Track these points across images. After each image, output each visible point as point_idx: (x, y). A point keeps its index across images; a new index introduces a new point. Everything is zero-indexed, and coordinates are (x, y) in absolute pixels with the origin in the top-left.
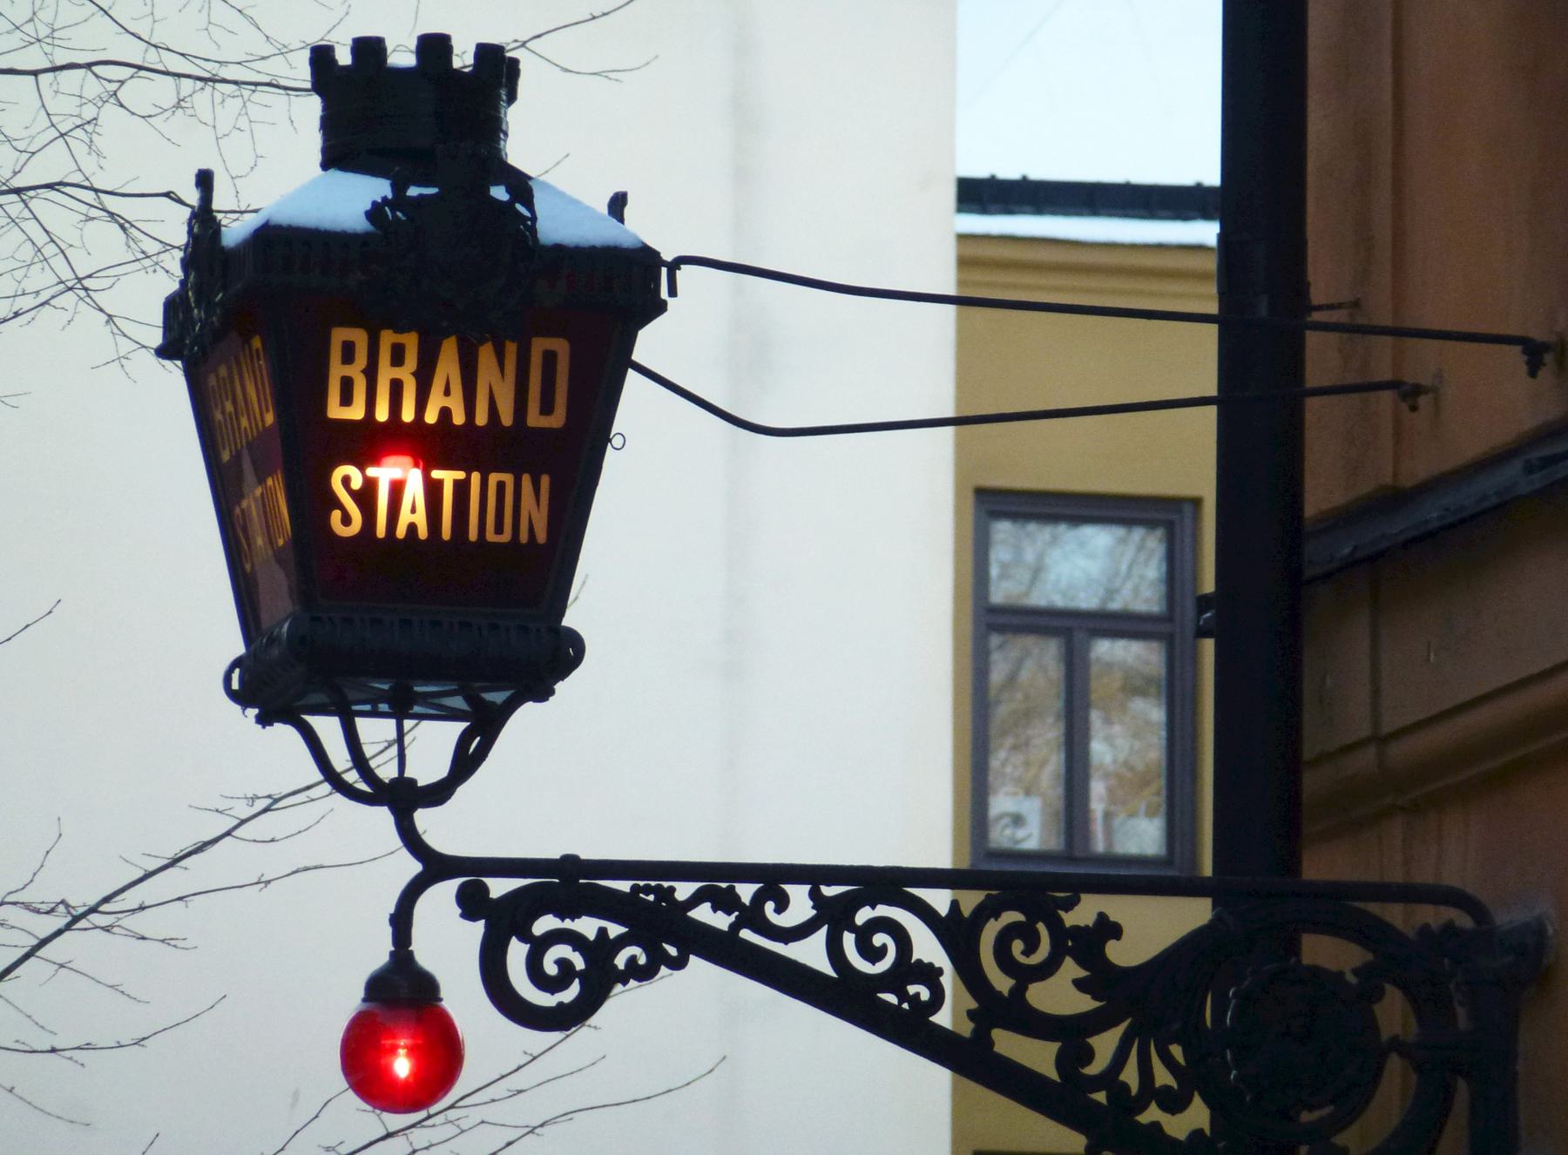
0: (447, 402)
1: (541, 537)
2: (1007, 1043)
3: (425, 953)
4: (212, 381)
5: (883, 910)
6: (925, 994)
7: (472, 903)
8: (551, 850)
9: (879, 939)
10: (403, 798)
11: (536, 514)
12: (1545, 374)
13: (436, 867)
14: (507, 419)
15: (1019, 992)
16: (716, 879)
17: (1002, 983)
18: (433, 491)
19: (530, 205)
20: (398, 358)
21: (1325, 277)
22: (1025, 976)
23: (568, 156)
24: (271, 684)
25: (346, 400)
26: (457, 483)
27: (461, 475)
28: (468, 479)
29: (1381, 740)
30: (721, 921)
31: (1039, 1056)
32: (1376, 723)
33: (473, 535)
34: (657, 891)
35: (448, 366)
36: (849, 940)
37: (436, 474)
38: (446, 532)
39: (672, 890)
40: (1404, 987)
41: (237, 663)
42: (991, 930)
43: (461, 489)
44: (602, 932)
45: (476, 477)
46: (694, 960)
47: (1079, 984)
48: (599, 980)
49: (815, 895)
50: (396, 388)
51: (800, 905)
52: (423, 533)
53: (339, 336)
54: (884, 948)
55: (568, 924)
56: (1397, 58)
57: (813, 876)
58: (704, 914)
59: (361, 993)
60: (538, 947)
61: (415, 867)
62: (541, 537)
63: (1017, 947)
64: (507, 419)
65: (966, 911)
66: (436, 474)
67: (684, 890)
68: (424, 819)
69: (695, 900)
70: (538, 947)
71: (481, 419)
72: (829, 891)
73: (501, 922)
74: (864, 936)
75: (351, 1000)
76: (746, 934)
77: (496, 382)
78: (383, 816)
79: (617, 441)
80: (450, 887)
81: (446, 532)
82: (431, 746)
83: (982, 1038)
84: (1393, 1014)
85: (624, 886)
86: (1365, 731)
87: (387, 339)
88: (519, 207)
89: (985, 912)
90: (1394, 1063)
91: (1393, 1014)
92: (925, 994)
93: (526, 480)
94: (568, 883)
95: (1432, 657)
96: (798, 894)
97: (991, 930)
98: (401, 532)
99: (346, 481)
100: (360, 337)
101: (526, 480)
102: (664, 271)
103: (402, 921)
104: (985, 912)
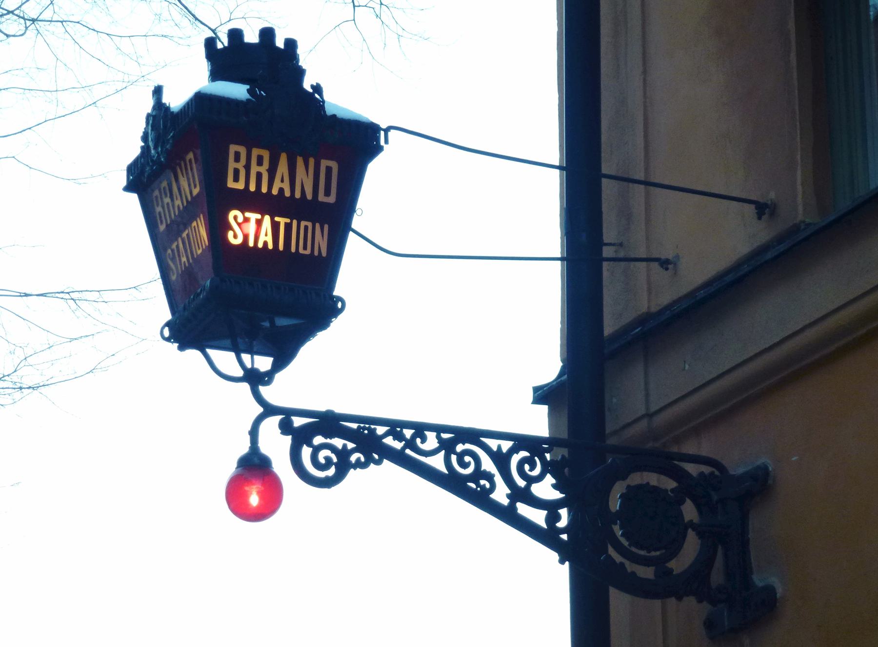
0: (282, 185)
1: (324, 254)
2: (523, 509)
3: (264, 448)
4: (159, 209)
5: (468, 446)
6: (488, 485)
7: (286, 427)
8: (322, 408)
9: (467, 459)
10: (255, 379)
11: (322, 243)
12: (765, 217)
13: (269, 410)
14: (309, 196)
15: (528, 487)
16: (395, 427)
17: (521, 483)
18: (275, 226)
19: (321, 94)
20: (260, 162)
21: (609, 234)
22: (530, 480)
23: (340, 81)
24: (191, 328)
25: (236, 179)
26: (286, 224)
27: (288, 220)
28: (292, 222)
29: (649, 416)
30: (398, 445)
31: (538, 517)
32: (647, 408)
33: (293, 250)
34: (369, 429)
35: (283, 168)
36: (454, 458)
37: (277, 219)
38: (281, 247)
39: (375, 429)
40: (694, 501)
41: (168, 324)
42: (515, 459)
43: (288, 227)
44: (345, 446)
45: (295, 222)
46: (385, 461)
47: (555, 486)
48: (343, 466)
49: (438, 437)
50: (259, 176)
51: (431, 441)
52: (270, 246)
53: (233, 148)
54: (469, 463)
55: (328, 441)
56: (646, 136)
57: (439, 429)
58: (389, 441)
59: (235, 465)
60: (316, 450)
61: (260, 410)
62: (324, 254)
63: (527, 467)
64: (309, 196)
65: (505, 450)
66: (277, 219)
67: (381, 430)
68: (263, 389)
69: (386, 435)
70: (316, 450)
71: (298, 195)
72: (445, 436)
73: (301, 437)
74: (460, 456)
75: (230, 468)
76: (408, 451)
77: (305, 178)
78: (245, 387)
79: (358, 212)
80: (277, 419)
81: (281, 247)
82: (264, 363)
83: (512, 507)
84: (689, 511)
85: (354, 426)
86: (642, 411)
87: (255, 152)
88: (316, 95)
89: (513, 450)
90: (691, 535)
91: (689, 511)
92: (488, 485)
93: (318, 226)
94: (328, 423)
95: (687, 367)
96: (431, 436)
97: (515, 459)
98: (260, 245)
99: (235, 218)
100: (242, 150)
101: (318, 226)
102: (382, 133)
103: (254, 433)
104: (513, 450)
